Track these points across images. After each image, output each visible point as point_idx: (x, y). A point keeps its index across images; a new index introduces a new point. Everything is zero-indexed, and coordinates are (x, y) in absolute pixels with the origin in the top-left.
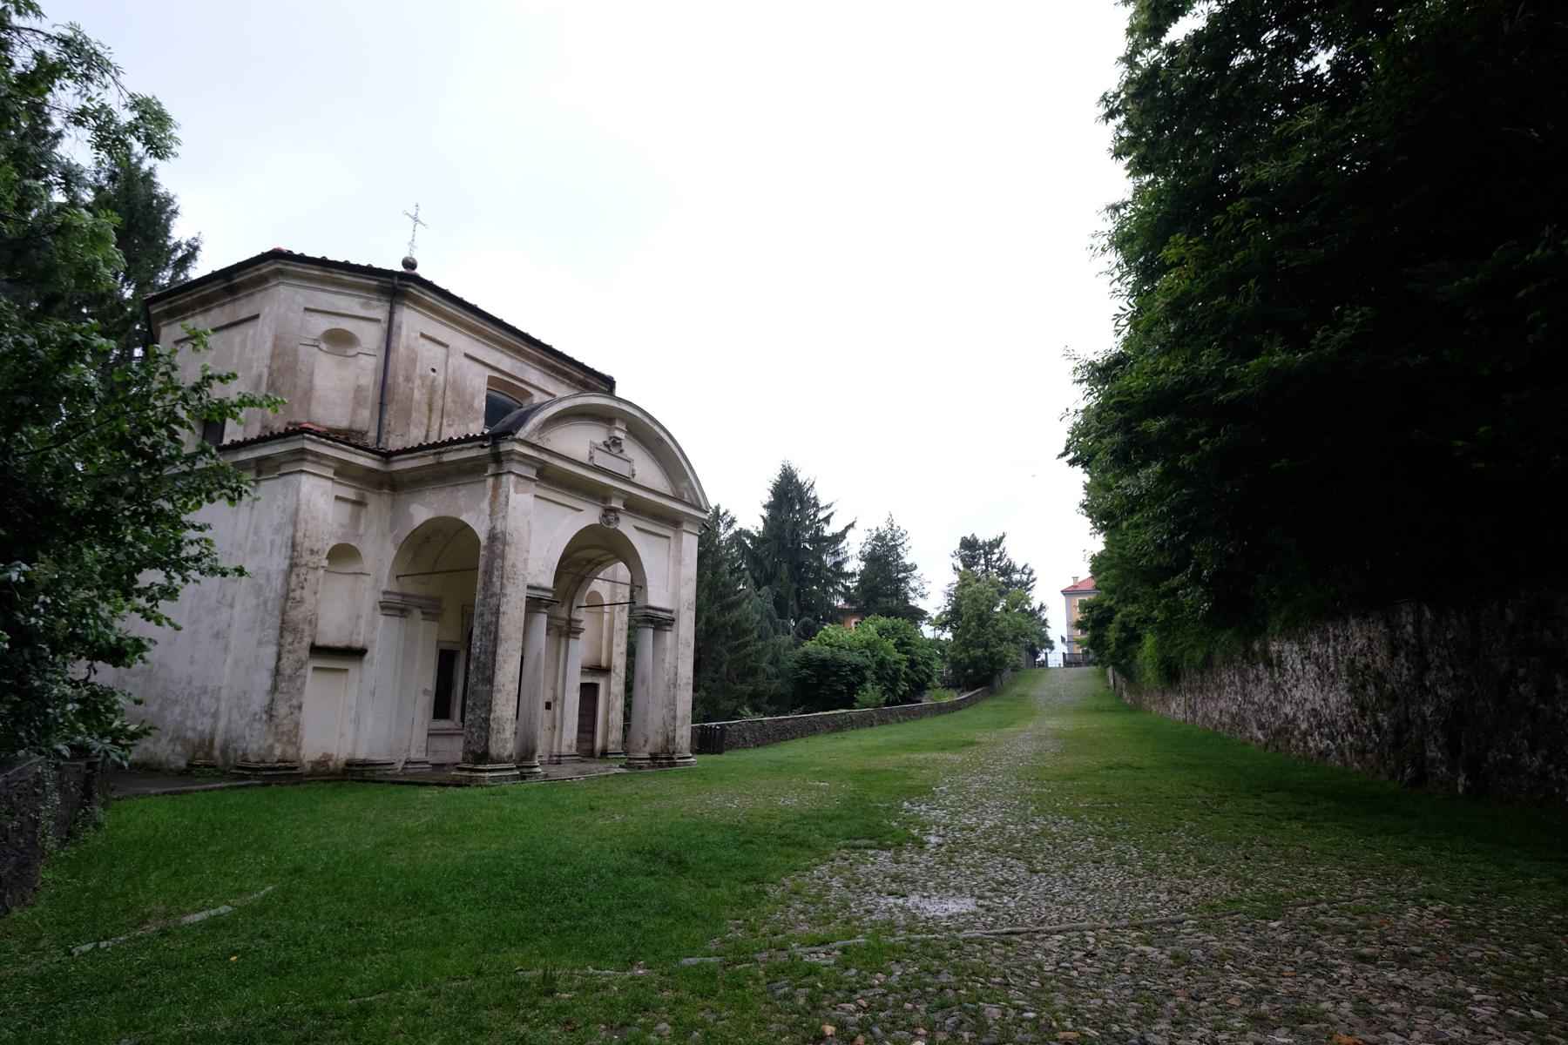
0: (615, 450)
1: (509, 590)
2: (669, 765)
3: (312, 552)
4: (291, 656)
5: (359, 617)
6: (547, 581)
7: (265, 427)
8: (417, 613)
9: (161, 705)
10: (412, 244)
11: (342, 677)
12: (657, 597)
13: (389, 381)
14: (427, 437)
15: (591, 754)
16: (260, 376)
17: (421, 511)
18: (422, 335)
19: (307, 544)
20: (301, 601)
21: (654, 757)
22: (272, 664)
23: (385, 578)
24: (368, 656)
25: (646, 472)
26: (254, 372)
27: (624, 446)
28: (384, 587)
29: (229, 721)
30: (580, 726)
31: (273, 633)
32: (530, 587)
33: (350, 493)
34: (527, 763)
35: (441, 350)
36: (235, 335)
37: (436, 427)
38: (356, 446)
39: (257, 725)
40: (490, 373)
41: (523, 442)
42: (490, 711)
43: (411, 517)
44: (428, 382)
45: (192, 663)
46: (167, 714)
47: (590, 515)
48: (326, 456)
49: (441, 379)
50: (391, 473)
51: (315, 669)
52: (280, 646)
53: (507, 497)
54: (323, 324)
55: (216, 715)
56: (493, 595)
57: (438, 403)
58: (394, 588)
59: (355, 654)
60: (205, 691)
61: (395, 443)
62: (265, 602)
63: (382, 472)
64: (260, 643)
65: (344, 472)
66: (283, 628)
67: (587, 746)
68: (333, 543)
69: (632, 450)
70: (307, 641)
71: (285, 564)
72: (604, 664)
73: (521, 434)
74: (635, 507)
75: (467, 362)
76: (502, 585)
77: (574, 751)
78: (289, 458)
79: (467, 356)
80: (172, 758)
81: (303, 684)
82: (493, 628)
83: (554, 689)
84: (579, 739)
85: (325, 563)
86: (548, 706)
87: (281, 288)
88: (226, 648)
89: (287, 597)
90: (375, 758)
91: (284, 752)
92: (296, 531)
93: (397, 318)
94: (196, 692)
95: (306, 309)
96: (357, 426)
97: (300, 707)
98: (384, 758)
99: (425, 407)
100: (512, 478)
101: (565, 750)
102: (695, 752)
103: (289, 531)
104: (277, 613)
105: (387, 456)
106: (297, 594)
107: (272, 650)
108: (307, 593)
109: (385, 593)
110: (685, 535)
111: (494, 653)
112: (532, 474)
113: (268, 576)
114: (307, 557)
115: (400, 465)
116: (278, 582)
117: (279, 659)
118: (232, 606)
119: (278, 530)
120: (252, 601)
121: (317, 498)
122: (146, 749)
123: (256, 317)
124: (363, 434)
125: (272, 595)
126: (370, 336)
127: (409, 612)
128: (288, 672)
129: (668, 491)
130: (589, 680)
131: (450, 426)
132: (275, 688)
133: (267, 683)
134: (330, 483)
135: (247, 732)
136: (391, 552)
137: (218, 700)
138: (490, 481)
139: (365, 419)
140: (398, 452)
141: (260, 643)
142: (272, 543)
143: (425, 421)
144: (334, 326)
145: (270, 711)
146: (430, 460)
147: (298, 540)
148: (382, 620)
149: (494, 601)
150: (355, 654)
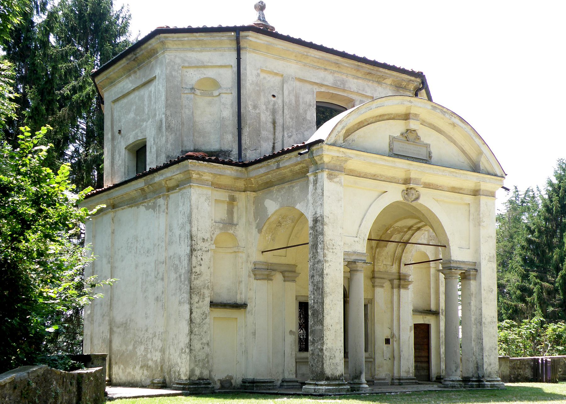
2: (479, 386)
4: (198, 310)
7: (168, 157)
9: (134, 345)
12: (459, 254)
13: (242, 110)
14: (274, 148)
15: (428, 379)
16: (161, 121)
19: (200, 235)
21: (466, 380)
26: (157, 118)
30: (415, 357)
31: (186, 296)
33: (224, 195)
34: (356, 381)
35: (279, 79)
36: (144, 92)
38: (223, 163)
39: (184, 356)
42: (323, 344)
44: (271, 107)
45: (147, 317)
47: (395, 194)
49: (280, 102)
52: (191, 304)
56: (319, 261)
57: (279, 121)
61: (250, 155)
62: (180, 276)
66: (192, 291)
67: (423, 373)
70: (207, 300)
71: (188, 251)
72: (433, 308)
76: (324, 256)
77: (412, 375)
80: (143, 378)
82: (320, 285)
83: (391, 328)
84: (416, 367)
85: (213, 247)
86: (387, 341)
89: (191, 272)
90: (259, 378)
91: (201, 373)
92: (191, 227)
94: (151, 336)
96: (226, 148)
98: (266, 378)
99: (270, 126)
101: (403, 375)
103: (188, 228)
104: (187, 282)
106: (197, 269)
107: (187, 307)
108: (203, 268)
111: (323, 303)
113: (180, 258)
114: (201, 245)
116: (185, 263)
117: (191, 313)
118: (162, 279)
119: (183, 227)
122: (129, 373)
124: (226, 153)
125: (183, 271)
126: (227, 78)
128: (198, 321)
130: (421, 320)
131: (290, 137)
132: (191, 332)
133: (186, 329)
135: (179, 361)
143: (271, 137)
144: (203, 76)
145: (190, 345)
147: (194, 233)
149: (319, 266)
150: (240, 306)
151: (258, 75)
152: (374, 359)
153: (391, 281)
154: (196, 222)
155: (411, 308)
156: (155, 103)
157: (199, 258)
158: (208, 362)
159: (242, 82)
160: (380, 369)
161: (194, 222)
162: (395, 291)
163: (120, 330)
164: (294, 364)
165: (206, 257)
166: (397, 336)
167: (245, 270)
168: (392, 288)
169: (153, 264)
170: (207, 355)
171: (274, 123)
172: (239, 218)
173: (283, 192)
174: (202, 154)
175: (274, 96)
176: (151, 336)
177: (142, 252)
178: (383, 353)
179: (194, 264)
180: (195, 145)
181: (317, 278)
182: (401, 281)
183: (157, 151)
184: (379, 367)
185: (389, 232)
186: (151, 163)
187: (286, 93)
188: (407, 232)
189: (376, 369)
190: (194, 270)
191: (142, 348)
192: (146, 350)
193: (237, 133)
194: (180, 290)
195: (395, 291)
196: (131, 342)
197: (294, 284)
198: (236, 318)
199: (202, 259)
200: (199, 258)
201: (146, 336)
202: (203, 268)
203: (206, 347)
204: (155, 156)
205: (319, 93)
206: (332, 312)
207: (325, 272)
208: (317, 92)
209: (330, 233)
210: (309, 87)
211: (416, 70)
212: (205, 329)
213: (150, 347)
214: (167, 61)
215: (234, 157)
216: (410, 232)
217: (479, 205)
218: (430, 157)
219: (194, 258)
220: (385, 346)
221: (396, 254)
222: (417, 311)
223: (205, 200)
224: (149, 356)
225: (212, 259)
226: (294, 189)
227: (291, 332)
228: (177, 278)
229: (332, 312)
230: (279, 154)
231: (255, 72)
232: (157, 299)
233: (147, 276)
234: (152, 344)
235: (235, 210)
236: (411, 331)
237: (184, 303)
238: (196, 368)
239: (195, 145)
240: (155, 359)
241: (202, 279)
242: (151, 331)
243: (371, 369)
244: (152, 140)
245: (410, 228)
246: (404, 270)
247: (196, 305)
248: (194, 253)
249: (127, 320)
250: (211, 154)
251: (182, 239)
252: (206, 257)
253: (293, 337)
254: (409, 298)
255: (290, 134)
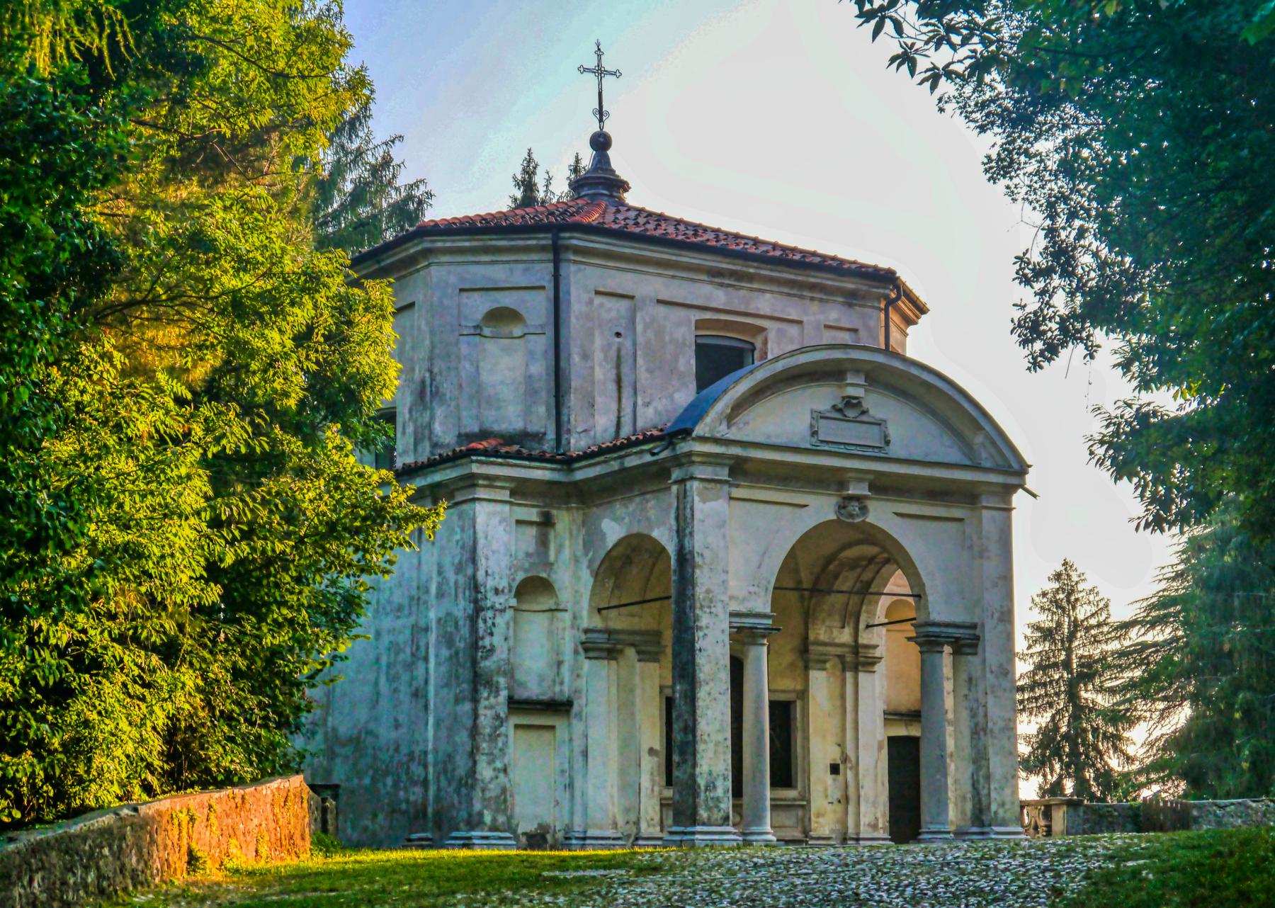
0: (851, 414)
1: (704, 620)
3: (497, 591)
5: (560, 663)
6: (762, 604)
8: (631, 652)
10: (601, 114)
11: (547, 735)
16: (423, 382)
17: (613, 528)
18: (598, 293)
19: (490, 583)
20: (492, 650)
22: (469, 723)
23: (585, 613)
24: (575, 709)
25: (909, 434)
27: (865, 405)
28: (585, 623)
29: (439, 789)
32: (732, 615)
33: (533, 514)
35: (623, 305)
37: (627, 409)
38: (530, 458)
40: (697, 315)
41: (703, 439)
42: (694, 765)
43: (603, 536)
46: (380, 785)
48: (497, 478)
50: (576, 483)
51: (517, 727)
53: (692, 509)
54: (479, 305)
55: (425, 783)
58: (597, 623)
59: (560, 707)
60: (411, 756)
61: (577, 443)
62: (457, 653)
63: (569, 482)
64: (457, 700)
65: (521, 490)
68: (520, 576)
69: (879, 405)
73: (699, 430)
74: (884, 487)
75: (662, 310)
78: (461, 484)
79: (659, 302)
81: (505, 743)
85: (513, 602)
86: (835, 769)
87: (433, 269)
88: (426, 707)
92: (476, 570)
93: (563, 271)
95: (461, 290)
96: (534, 428)
97: (505, 770)
99: (612, 387)
100: (696, 484)
102: (795, 787)
103: (470, 572)
104: (468, 664)
105: (568, 462)
106: (487, 642)
108: (497, 640)
109: (586, 631)
110: (985, 513)
112: (723, 474)
113: (456, 623)
114: (492, 599)
115: (583, 474)
116: (465, 631)
118: (426, 659)
120: (445, 653)
121: (497, 531)
122: (365, 829)
123: (412, 305)
124: (539, 437)
125: (462, 645)
126: (536, 307)
127: (621, 651)
129: (955, 456)
130: (900, 731)
131: (647, 405)
134: (507, 508)
136: (587, 579)
137: (425, 767)
138: (675, 488)
139: (541, 420)
140: (578, 459)
141: (457, 700)
142: (456, 583)
143: (614, 406)
144: (495, 305)
146: (615, 466)
148: (587, 665)
150: (560, 707)
151: (590, 302)
152: (809, 802)
153: (841, 657)
154: (483, 561)
155: (881, 706)
156: (413, 348)
157: (490, 622)
158: (505, 801)
159: (563, 315)
160: (821, 820)
161: (482, 563)
162: (849, 675)
163: (348, 751)
164: (658, 808)
165: (500, 620)
166: (853, 759)
167: (568, 642)
168: (844, 670)
169: (408, 632)
170: (504, 790)
171: (619, 382)
172: (560, 550)
173: (631, 509)
174: (493, 442)
175: (618, 335)
176: (405, 759)
177: (388, 609)
178: (826, 790)
179: (481, 633)
180: (481, 424)
181: (685, 657)
182: (858, 660)
183: (416, 433)
184: (818, 816)
185: (831, 567)
186: (405, 452)
187: (639, 328)
188: (866, 566)
189: (813, 818)
190: (480, 643)
191: (389, 781)
192: (396, 784)
193: (552, 401)
194: (457, 677)
195: (849, 675)
196: (367, 772)
197: (656, 665)
198: (553, 728)
199: (494, 624)
200: (490, 622)
201: (396, 759)
202: (497, 640)
203: (502, 775)
204: (412, 440)
205: (700, 324)
206: (709, 712)
207: (697, 646)
208: (697, 321)
209: (704, 580)
210: (681, 313)
211: (883, 264)
212: (500, 744)
213: (404, 778)
214: (435, 280)
215: (548, 446)
216: (873, 567)
217: (980, 521)
218: (888, 443)
219: (481, 624)
220: (829, 778)
221: (850, 607)
222: (892, 716)
223: (500, 522)
224: (402, 794)
225: (512, 624)
226: (649, 505)
227: (652, 751)
228: (451, 657)
229: (709, 712)
230: (622, 447)
231: (585, 297)
232: (416, 694)
233: (397, 653)
234: (407, 773)
235: (552, 536)
236: (880, 748)
237: (464, 699)
238: (486, 812)
239: (481, 424)
240: (412, 798)
241: (495, 658)
242: (404, 750)
243: (803, 820)
244: (406, 411)
245: (871, 560)
246: (864, 639)
247: (483, 703)
248: (482, 614)
249: (360, 732)
250: (509, 439)
251: (460, 590)
252: (500, 620)
253: (656, 759)
254: (877, 691)
255: (647, 400)
